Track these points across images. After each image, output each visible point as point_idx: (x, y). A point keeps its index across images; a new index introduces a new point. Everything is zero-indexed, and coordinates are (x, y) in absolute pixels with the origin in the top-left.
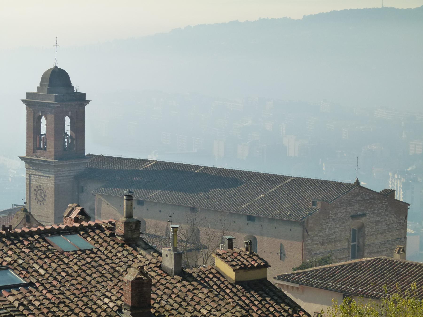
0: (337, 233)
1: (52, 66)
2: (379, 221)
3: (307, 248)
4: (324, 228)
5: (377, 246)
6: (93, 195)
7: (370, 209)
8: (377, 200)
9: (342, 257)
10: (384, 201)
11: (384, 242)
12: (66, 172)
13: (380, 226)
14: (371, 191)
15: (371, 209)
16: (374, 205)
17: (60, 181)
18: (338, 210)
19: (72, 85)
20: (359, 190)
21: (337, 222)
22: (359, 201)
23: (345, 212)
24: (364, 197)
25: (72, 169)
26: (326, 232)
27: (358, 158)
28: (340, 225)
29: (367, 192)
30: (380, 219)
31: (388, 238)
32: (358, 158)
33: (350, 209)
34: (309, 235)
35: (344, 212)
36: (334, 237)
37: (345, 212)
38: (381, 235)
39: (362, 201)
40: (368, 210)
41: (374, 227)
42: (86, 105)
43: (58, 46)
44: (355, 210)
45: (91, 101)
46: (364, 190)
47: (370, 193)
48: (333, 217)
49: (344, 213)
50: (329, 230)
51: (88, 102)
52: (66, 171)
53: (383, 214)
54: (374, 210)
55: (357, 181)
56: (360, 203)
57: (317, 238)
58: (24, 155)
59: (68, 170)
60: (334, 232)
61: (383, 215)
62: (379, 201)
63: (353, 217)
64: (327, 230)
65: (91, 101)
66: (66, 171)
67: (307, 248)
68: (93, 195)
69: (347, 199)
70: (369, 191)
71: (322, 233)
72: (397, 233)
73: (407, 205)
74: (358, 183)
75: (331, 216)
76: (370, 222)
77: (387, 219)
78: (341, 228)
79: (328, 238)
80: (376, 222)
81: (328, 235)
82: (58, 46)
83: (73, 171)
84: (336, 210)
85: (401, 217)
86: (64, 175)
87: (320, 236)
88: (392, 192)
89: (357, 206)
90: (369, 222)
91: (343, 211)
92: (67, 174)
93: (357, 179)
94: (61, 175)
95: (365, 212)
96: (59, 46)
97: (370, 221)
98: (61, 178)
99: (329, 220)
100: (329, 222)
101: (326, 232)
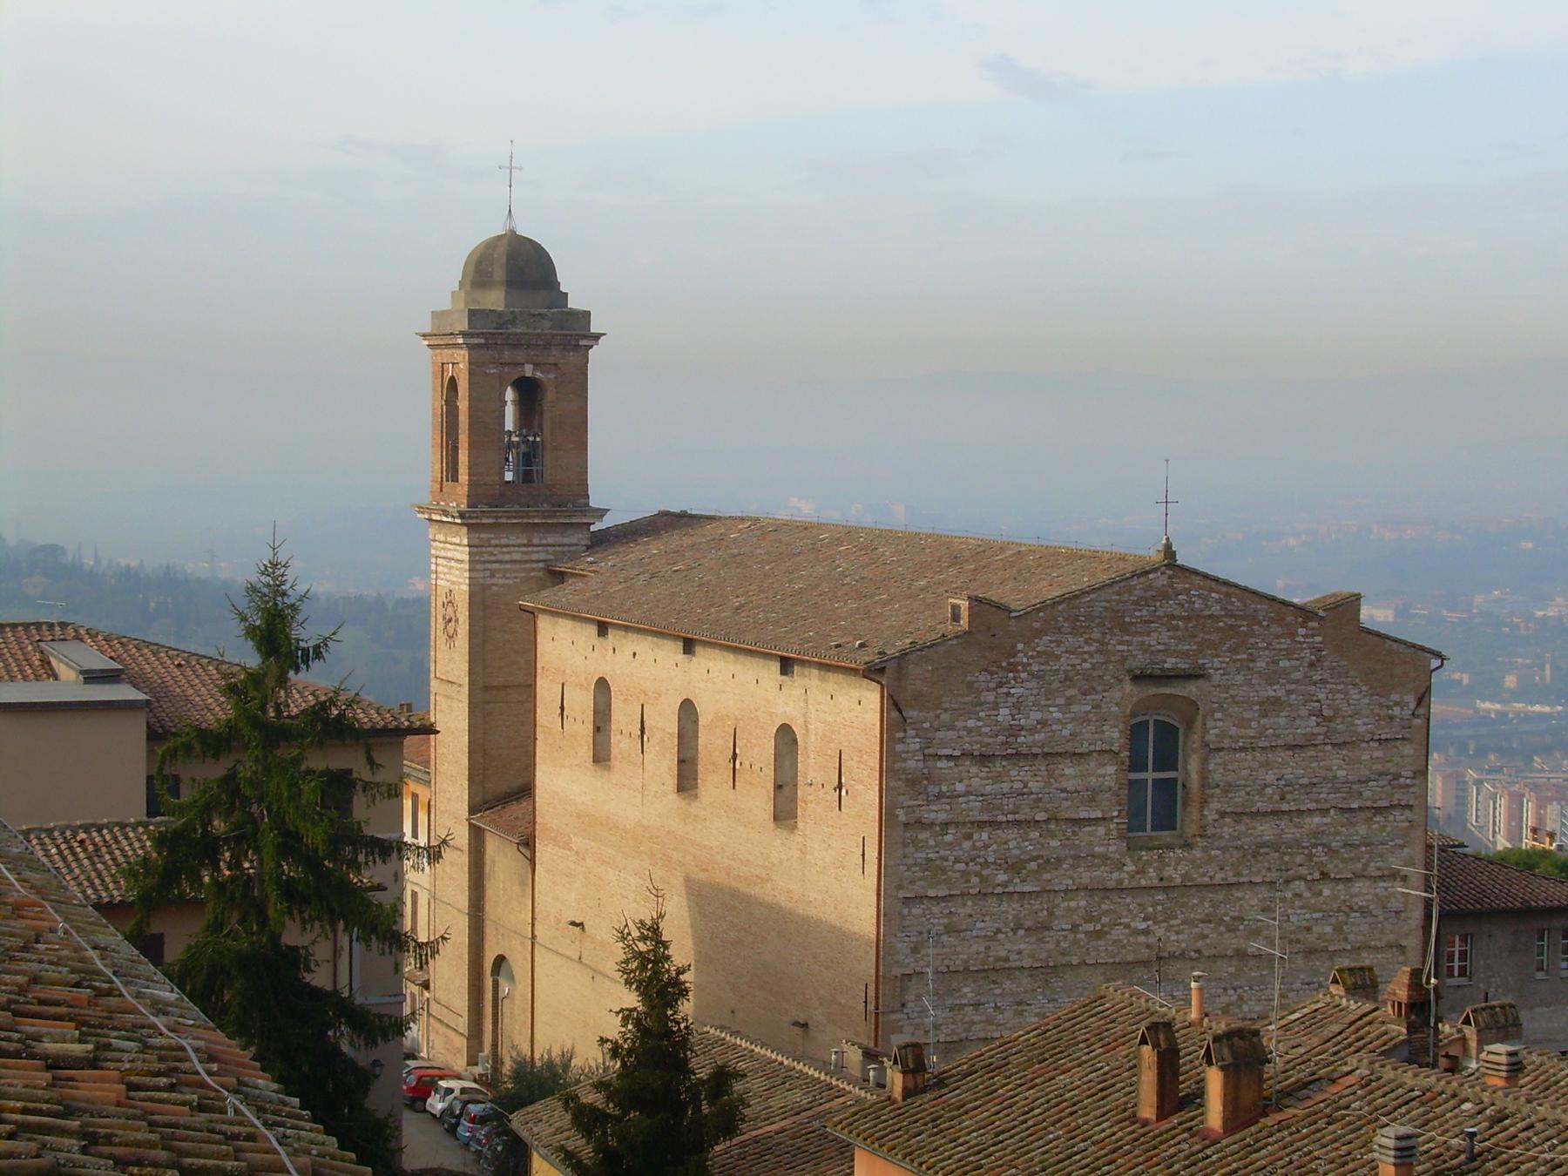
0: (1054, 727)
1: (495, 228)
2: (1276, 701)
3: (897, 766)
4: (985, 703)
5: (1269, 791)
6: (521, 609)
7: (1228, 654)
8: (1265, 623)
9: (1083, 815)
10: (1301, 631)
11: (1305, 781)
12: (512, 549)
13: (1282, 721)
14: (1233, 589)
15: (1238, 654)
16: (1252, 640)
17: (492, 576)
18: (1059, 643)
19: (563, 289)
20: (1170, 577)
21: (1056, 685)
22: (1173, 617)
23: (1099, 651)
24: (1197, 606)
25: (536, 541)
26: (1000, 718)
27: (1167, 461)
28: (1070, 701)
29: (1211, 590)
30: (1281, 693)
31: (1328, 769)
32: (1167, 461)
33: (1120, 643)
34: (908, 721)
35: (1091, 655)
36: (1040, 737)
37: (1099, 651)
38: (1291, 753)
39: (1187, 619)
40: (1217, 656)
41: (1250, 720)
42: (591, 347)
43: (516, 168)
44: (1153, 648)
45: (604, 334)
46: (1197, 580)
47: (1228, 595)
48: (1035, 668)
49: (1091, 656)
50: (1014, 711)
51: (597, 337)
52: (514, 546)
53: (1296, 675)
54: (1252, 659)
55: (1168, 547)
56: (1177, 628)
57: (952, 734)
58: (426, 499)
59: (520, 541)
60: (1043, 723)
61: (1297, 682)
62: (1275, 629)
63: (1139, 678)
64: (1004, 711)
65: (604, 334)
66: (514, 546)
67: (897, 766)
68: (521, 609)
69: (1107, 605)
70: (1224, 589)
71: (979, 719)
72: (1376, 754)
73: (1428, 655)
74: (1169, 552)
75: (1025, 660)
76: (1230, 700)
77: (1322, 696)
78: (1075, 708)
79: (1011, 739)
80: (1261, 703)
81: (1015, 731)
82: (516, 168)
83: (540, 548)
84: (1051, 641)
85: (1395, 697)
86: (507, 557)
87: (969, 731)
88: (1351, 604)
89: (1158, 638)
90: (1226, 698)
91: (1086, 649)
92: (517, 557)
93: (1168, 539)
94: (493, 558)
95: (1200, 662)
96: (521, 168)
97: (1233, 697)
98: (496, 566)
99: (1011, 675)
100: (1013, 682)
101: (1000, 718)
